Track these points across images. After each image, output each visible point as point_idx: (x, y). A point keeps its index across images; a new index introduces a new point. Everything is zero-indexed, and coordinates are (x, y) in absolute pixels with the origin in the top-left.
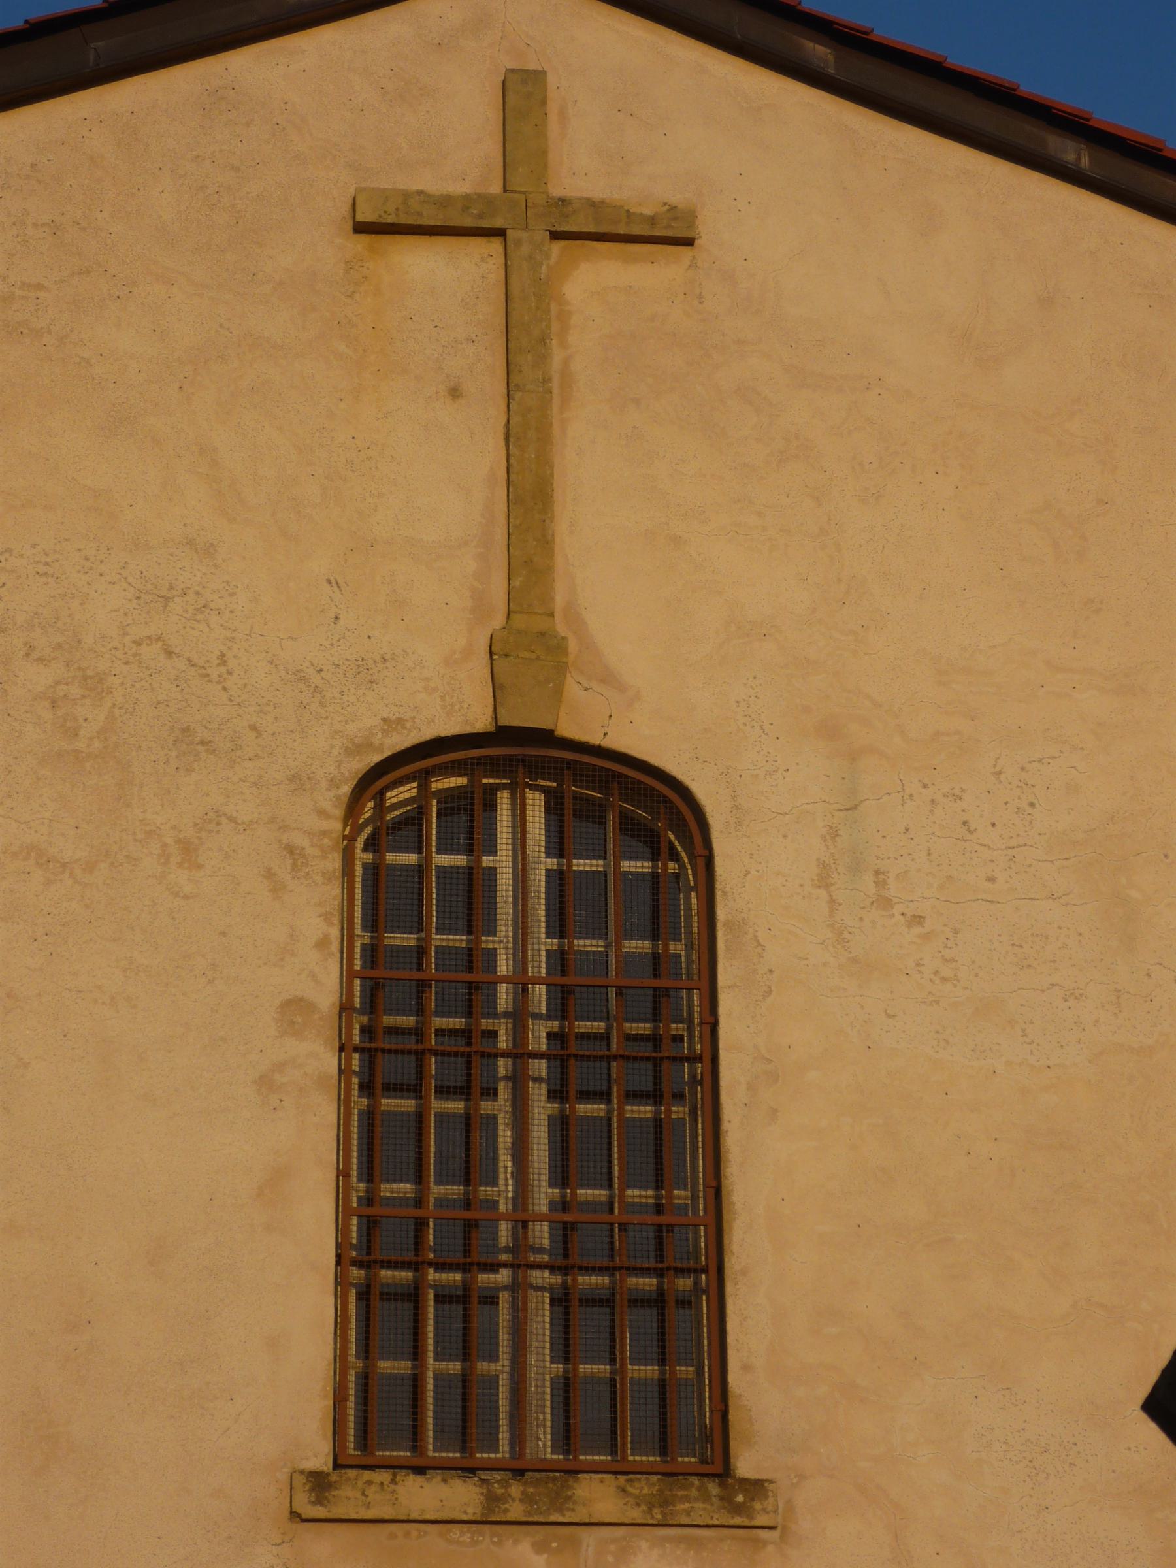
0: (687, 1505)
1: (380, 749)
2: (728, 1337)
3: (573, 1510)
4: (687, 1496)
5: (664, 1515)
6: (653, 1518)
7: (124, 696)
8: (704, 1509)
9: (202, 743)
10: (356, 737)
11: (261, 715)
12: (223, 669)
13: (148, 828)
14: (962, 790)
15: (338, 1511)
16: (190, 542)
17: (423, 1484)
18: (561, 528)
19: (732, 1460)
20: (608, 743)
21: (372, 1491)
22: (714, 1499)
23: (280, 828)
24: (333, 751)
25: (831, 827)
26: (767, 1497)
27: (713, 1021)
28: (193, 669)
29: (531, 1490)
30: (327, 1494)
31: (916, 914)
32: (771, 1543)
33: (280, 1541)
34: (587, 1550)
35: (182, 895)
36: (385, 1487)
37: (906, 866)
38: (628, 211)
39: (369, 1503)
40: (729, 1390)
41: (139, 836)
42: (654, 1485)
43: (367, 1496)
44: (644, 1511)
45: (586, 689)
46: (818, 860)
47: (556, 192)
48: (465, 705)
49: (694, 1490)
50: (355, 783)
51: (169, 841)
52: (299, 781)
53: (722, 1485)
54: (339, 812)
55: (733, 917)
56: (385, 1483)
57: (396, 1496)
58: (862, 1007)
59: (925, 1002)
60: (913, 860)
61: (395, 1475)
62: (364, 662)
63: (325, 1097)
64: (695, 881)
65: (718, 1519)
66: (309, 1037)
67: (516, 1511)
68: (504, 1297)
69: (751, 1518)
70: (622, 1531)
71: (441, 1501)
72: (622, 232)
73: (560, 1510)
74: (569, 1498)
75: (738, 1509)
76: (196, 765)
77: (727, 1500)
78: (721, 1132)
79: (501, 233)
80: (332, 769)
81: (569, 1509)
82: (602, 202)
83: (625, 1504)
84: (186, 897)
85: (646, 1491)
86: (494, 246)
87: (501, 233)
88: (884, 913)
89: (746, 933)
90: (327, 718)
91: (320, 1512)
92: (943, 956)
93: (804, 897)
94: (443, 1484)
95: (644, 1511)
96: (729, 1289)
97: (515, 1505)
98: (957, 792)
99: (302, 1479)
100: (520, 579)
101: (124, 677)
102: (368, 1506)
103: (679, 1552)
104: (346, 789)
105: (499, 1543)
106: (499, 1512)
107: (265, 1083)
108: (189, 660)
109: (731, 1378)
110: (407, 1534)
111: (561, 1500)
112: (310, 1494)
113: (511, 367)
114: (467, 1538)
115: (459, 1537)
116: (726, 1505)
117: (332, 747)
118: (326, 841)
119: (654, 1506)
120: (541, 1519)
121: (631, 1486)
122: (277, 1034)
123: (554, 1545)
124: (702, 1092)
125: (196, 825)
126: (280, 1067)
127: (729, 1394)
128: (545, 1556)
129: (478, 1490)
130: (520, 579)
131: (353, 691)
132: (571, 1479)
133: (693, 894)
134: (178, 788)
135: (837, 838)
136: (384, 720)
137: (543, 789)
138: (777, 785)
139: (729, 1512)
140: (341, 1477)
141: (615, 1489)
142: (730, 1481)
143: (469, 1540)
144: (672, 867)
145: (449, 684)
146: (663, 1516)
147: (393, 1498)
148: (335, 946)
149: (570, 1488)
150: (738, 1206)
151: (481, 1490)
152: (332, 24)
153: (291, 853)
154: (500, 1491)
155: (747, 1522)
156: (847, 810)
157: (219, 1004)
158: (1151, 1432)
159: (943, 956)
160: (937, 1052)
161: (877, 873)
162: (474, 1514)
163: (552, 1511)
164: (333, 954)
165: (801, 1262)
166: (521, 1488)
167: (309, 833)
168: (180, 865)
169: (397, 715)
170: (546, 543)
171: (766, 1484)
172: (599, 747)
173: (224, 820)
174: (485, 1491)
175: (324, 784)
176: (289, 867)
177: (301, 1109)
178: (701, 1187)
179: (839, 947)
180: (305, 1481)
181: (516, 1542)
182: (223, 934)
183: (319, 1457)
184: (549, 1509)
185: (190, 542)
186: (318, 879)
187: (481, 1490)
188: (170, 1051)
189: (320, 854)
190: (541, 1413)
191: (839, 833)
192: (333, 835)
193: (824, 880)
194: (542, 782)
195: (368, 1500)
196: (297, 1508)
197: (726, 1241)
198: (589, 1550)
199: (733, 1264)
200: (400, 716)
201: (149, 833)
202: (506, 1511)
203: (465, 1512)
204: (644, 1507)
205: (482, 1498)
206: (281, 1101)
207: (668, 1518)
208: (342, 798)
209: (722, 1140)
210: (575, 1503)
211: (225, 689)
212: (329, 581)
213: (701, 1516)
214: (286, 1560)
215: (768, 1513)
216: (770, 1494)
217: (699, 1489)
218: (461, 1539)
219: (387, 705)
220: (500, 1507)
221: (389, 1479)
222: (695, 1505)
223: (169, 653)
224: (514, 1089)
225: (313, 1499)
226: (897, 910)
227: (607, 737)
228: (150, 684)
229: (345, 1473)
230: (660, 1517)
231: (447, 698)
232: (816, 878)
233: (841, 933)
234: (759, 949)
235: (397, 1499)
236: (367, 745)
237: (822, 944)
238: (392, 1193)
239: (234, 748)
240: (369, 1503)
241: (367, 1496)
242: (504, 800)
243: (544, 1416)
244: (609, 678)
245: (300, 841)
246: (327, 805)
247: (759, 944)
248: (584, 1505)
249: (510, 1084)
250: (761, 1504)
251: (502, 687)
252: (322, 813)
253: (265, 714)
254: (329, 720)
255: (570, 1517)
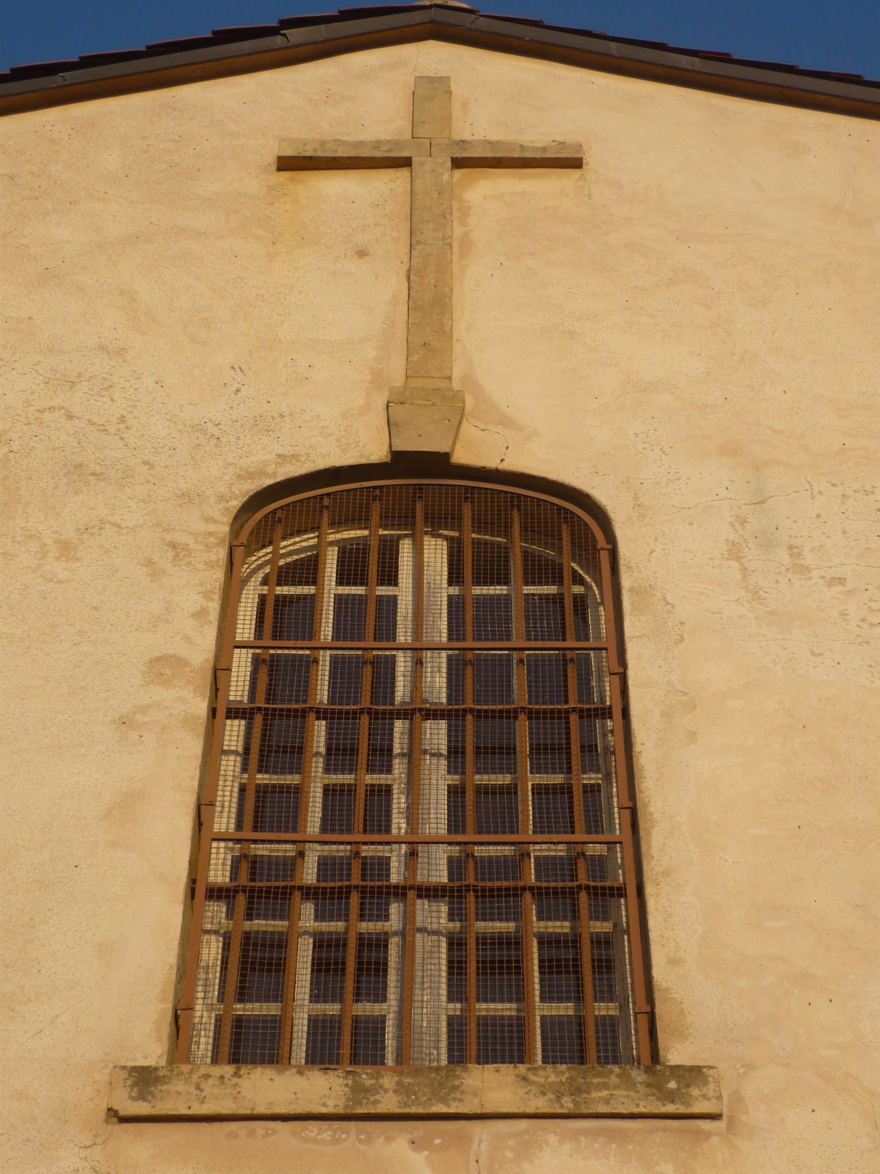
0: (605, 1093)
1: (274, 474)
2: (650, 933)
3: (461, 1100)
4: (604, 1083)
5: (576, 1104)
6: (562, 1106)
7: (21, 445)
8: (627, 1097)
9: (94, 474)
10: (249, 467)
11: (156, 454)
12: (122, 426)
13: (28, 533)
14: (873, 487)
16: (102, 348)
17: (273, 1077)
18: (460, 330)
19: (661, 1053)
20: (506, 466)
21: (207, 1086)
22: (639, 1086)
23: (164, 530)
24: (225, 477)
25: (739, 517)
26: (706, 1083)
27: (649, 1010)
28: (92, 426)
29: (409, 1080)
30: (152, 1088)
31: (836, 577)
32: (715, 1135)
33: (91, 1143)
34: (479, 1146)
35: (55, 580)
36: (226, 1080)
37: (820, 541)
38: (522, 146)
39: (205, 1097)
40: (654, 983)
41: (18, 539)
42: (563, 1073)
43: (202, 1090)
44: (550, 1100)
45: (483, 430)
46: (726, 540)
47: (456, 137)
48: (362, 444)
49: (613, 1077)
50: (245, 499)
51: (49, 542)
52: (186, 498)
53: (648, 1070)
54: (228, 519)
55: (639, 584)
56: (226, 1076)
57: (239, 1089)
58: (785, 649)
59: (854, 643)
60: (828, 537)
61: (239, 1069)
62: (262, 418)
63: (190, 733)
64: (601, 594)
65: (645, 1107)
66: (178, 685)
68: (394, 944)
69: (689, 1105)
70: (523, 1124)
71: (295, 1094)
72: (516, 156)
73: (444, 1101)
74: (455, 1088)
75: (671, 1096)
76: (85, 489)
77: (656, 1087)
78: (633, 754)
80: (223, 489)
81: (454, 1099)
82: (498, 142)
83: (526, 1093)
84: (60, 582)
85: (553, 1078)
88: (801, 577)
89: (653, 596)
90: (220, 455)
91: (142, 1108)
92: (869, 607)
93: (714, 567)
94: (298, 1076)
95: (550, 1100)
96: (649, 889)
97: (387, 1096)
98: (868, 488)
99: (124, 1074)
100: (418, 356)
101: (23, 433)
102: (203, 1101)
103: (596, 1146)
104: (236, 504)
105: (369, 1141)
106: (367, 1104)
108: (89, 421)
109: (656, 972)
110: (251, 1133)
112: (132, 1089)
113: (413, 231)
114: (326, 1136)
115: (317, 1135)
116: (654, 1091)
117: (224, 474)
118: (212, 539)
119: (563, 1095)
120: (421, 1110)
121: (534, 1074)
122: (143, 683)
123: (437, 1141)
124: (622, 852)
125: (78, 530)
127: (655, 988)
128: (426, 1153)
129: (341, 1081)
130: (418, 356)
131: (249, 437)
132: (458, 1068)
133: (601, 608)
134: (64, 505)
135: (745, 524)
136: (279, 456)
137: (446, 538)
138: (680, 489)
139: (658, 1099)
140: (172, 1071)
141: (514, 1078)
142: (659, 1067)
143: (329, 1138)
144: (578, 589)
145: (345, 431)
146: (575, 1105)
147: (235, 1092)
149: (457, 1077)
150: (657, 816)
151: (346, 1082)
152: (270, 71)
153: (174, 548)
154: (369, 1082)
155: (682, 1110)
156: (755, 504)
157: (83, 661)
159: (869, 607)
160: (873, 682)
161: (791, 547)
162: (336, 1106)
163: (434, 1101)
164: (210, 622)
165: (733, 863)
166: (396, 1079)
167: (194, 534)
168: (57, 559)
169: (292, 452)
170: (446, 335)
171: (705, 1070)
172: (497, 471)
173: (108, 526)
174: (350, 1082)
175: (213, 499)
176: (171, 558)
177: (161, 744)
178: (616, 810)
179: (755, 603)
180: (126, 1076)
181: (389, 1139)
182: (96, 608)
184: (430, 1099)
185: (102, 348)
186: (201, 566)
187: (346, 1082)
188: (24, 699)
189: (204, 548)
190: (434, 1048)
191: (748, 520)
192: (219, 535)
194: (445, 532)
195: (204, 1094)
197: (644, 846)
198: (482, 1145)
199: (652, 868)
200: (295, 453)
201: (29, 537)
202: (376, 1102)
203: (324, 1105)
204: (550, 1096)
205: (346, 1089)
206: (141, 737)
207: (582, 1107)
208: (232, 509)
209: (635, 760)
210: (462, 1092)
211: (122, 438)
212: (233, 368)
213: (623, 1103)
214: (95, 1163)
215: (708, 1099)
216: (710, 1079)
217: (619, 1076)
218: (318, 1137)
219: (282, 446)
220: (368, 1099)
221: (232, 1072)
222: (615, 1092)
223: (70, 417)
224: (410, 763)
225: (134, 1094)
226: (815, 574)
227: (504, 462)
228: (49, 437)
229: (177, 1067)
230: (571, 1105)
231: (343, 440)
232: (726, 553)
233: (757, 593)
234: (669, 607)
235: (239, 1093)
237: (736, 601)
238: (270, 852)
239: (125, 477)
240: (205, 1097)
241: (202, 1090)
242: (406, 549)
243: (438, 1052)
244: (505, 422)
245: (182, 538)
246: (217, 515)
247: (668, 603)
248: (475, 1095)
249: (405, 761)
250: (700, 1090)
251: (397, 425)
252: (208, 520)
253: (159, 453)
254: (224, 457)
255: (457, 1107)
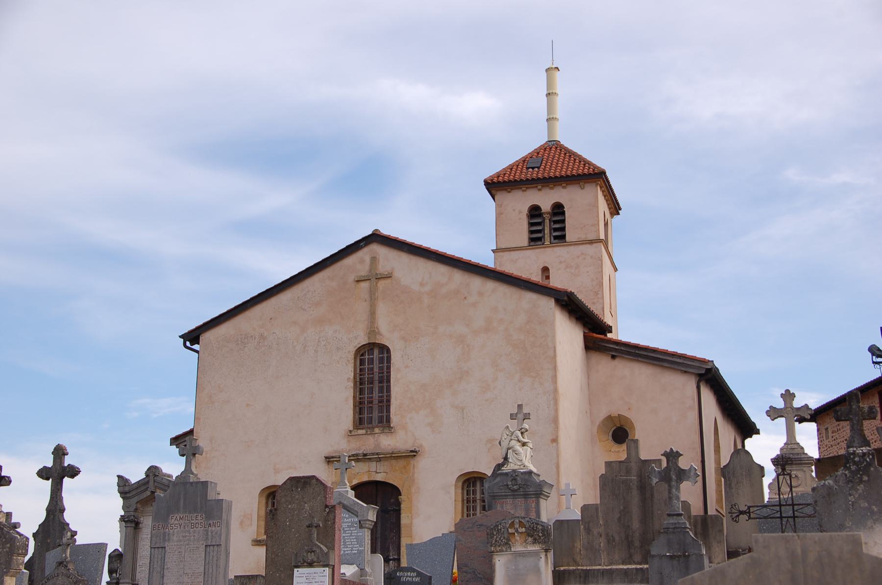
15: (353, 434)
67: (369, 433)
79: (370, 279)
86: (368, 281)
87: (370, 279)
107: (346, 388)
111: (373, 431)
126: (348, 386)
148: (353, 371)
170: (374, 319)
183: (351, 428)
193: (402, 357)
196: (874, 360)
236: (356, 347)
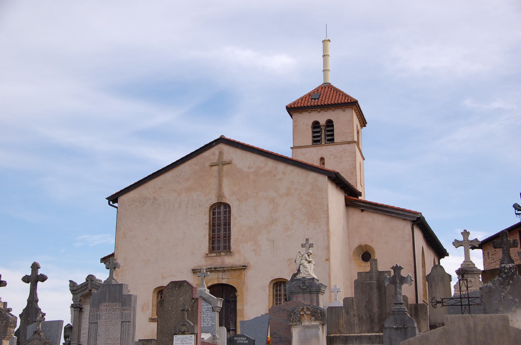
15: (208, 256)
67: (218, 255)
79: (218, 165)
86: (218, 166)
87: (218, 165)
107: (204, 229)
111: (221, 254)
126: (205, 227)
148: (208, 219)
158: (1, 274)
170: (221, 188)
183: (208, 253)
193: (238, 211)
196: (517, 212)
236: (210, 204)
